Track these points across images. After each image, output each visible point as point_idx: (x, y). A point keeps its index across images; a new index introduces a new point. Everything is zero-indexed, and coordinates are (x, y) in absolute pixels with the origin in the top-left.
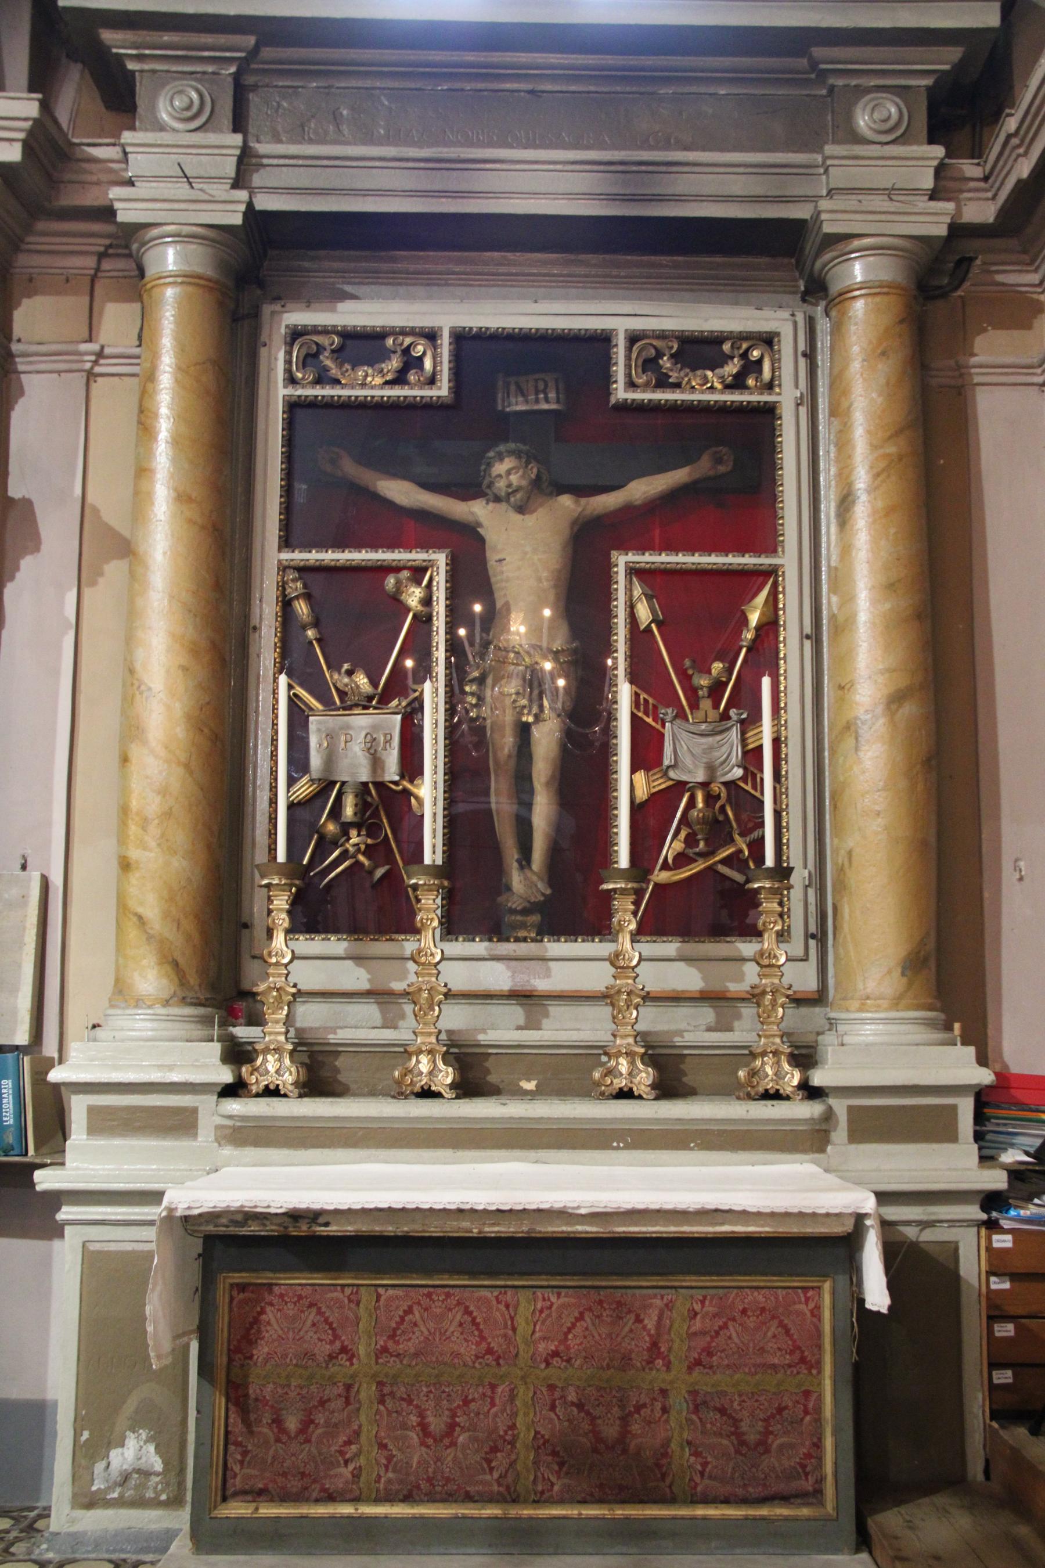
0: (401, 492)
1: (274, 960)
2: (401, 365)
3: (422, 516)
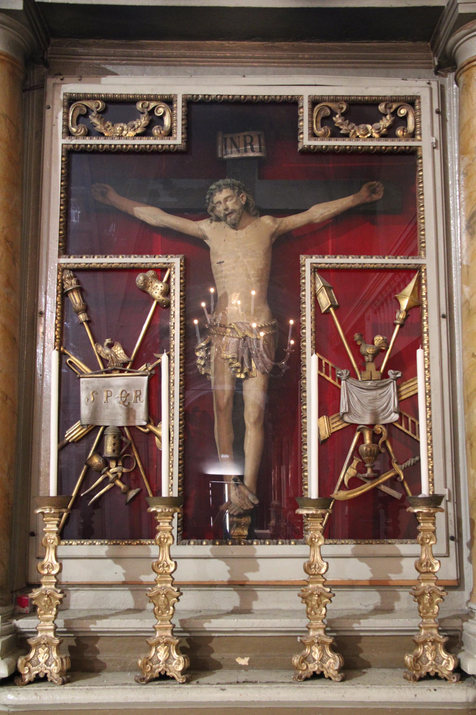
0: (150, 215)
1: (45, 572)
2: (148, 122)
3: (166, 231)
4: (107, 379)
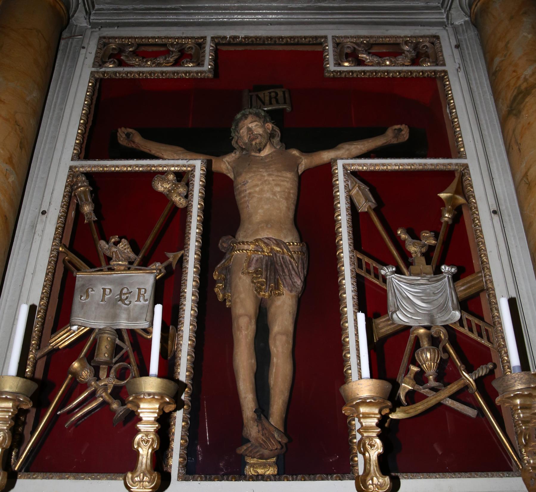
4: (109, 276)
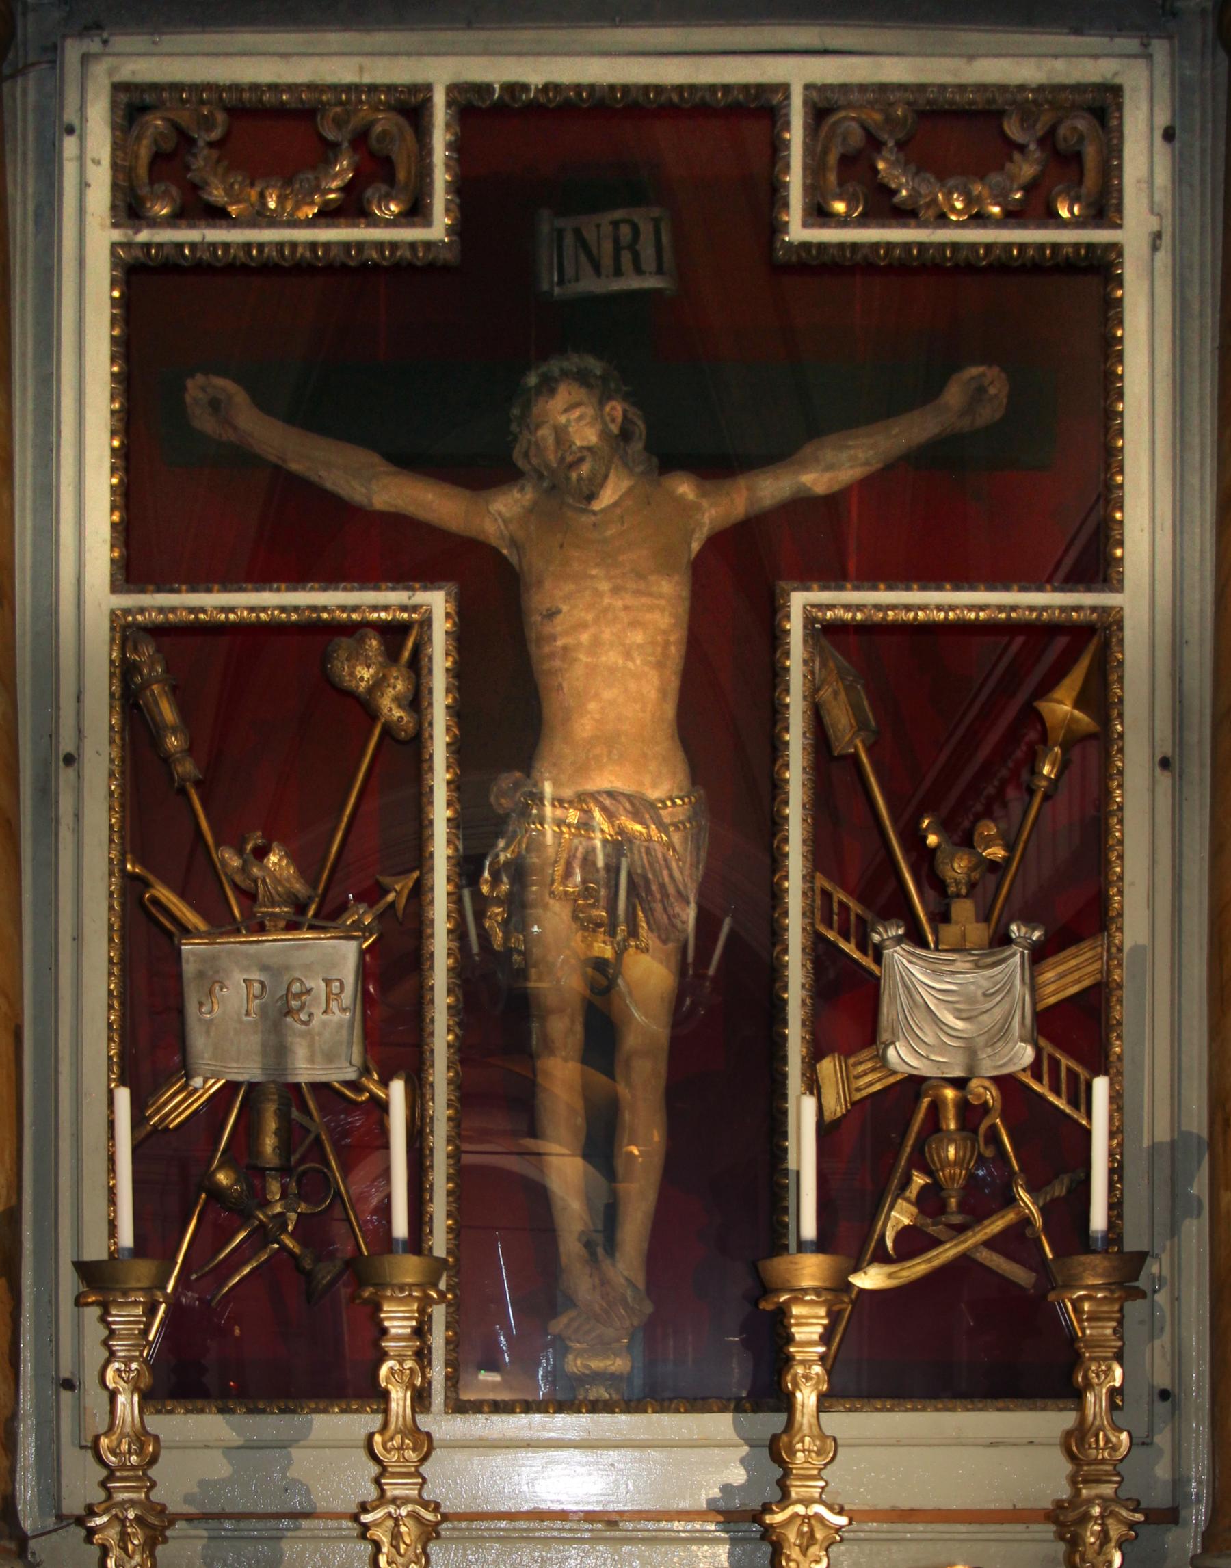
4: (255, 946)
